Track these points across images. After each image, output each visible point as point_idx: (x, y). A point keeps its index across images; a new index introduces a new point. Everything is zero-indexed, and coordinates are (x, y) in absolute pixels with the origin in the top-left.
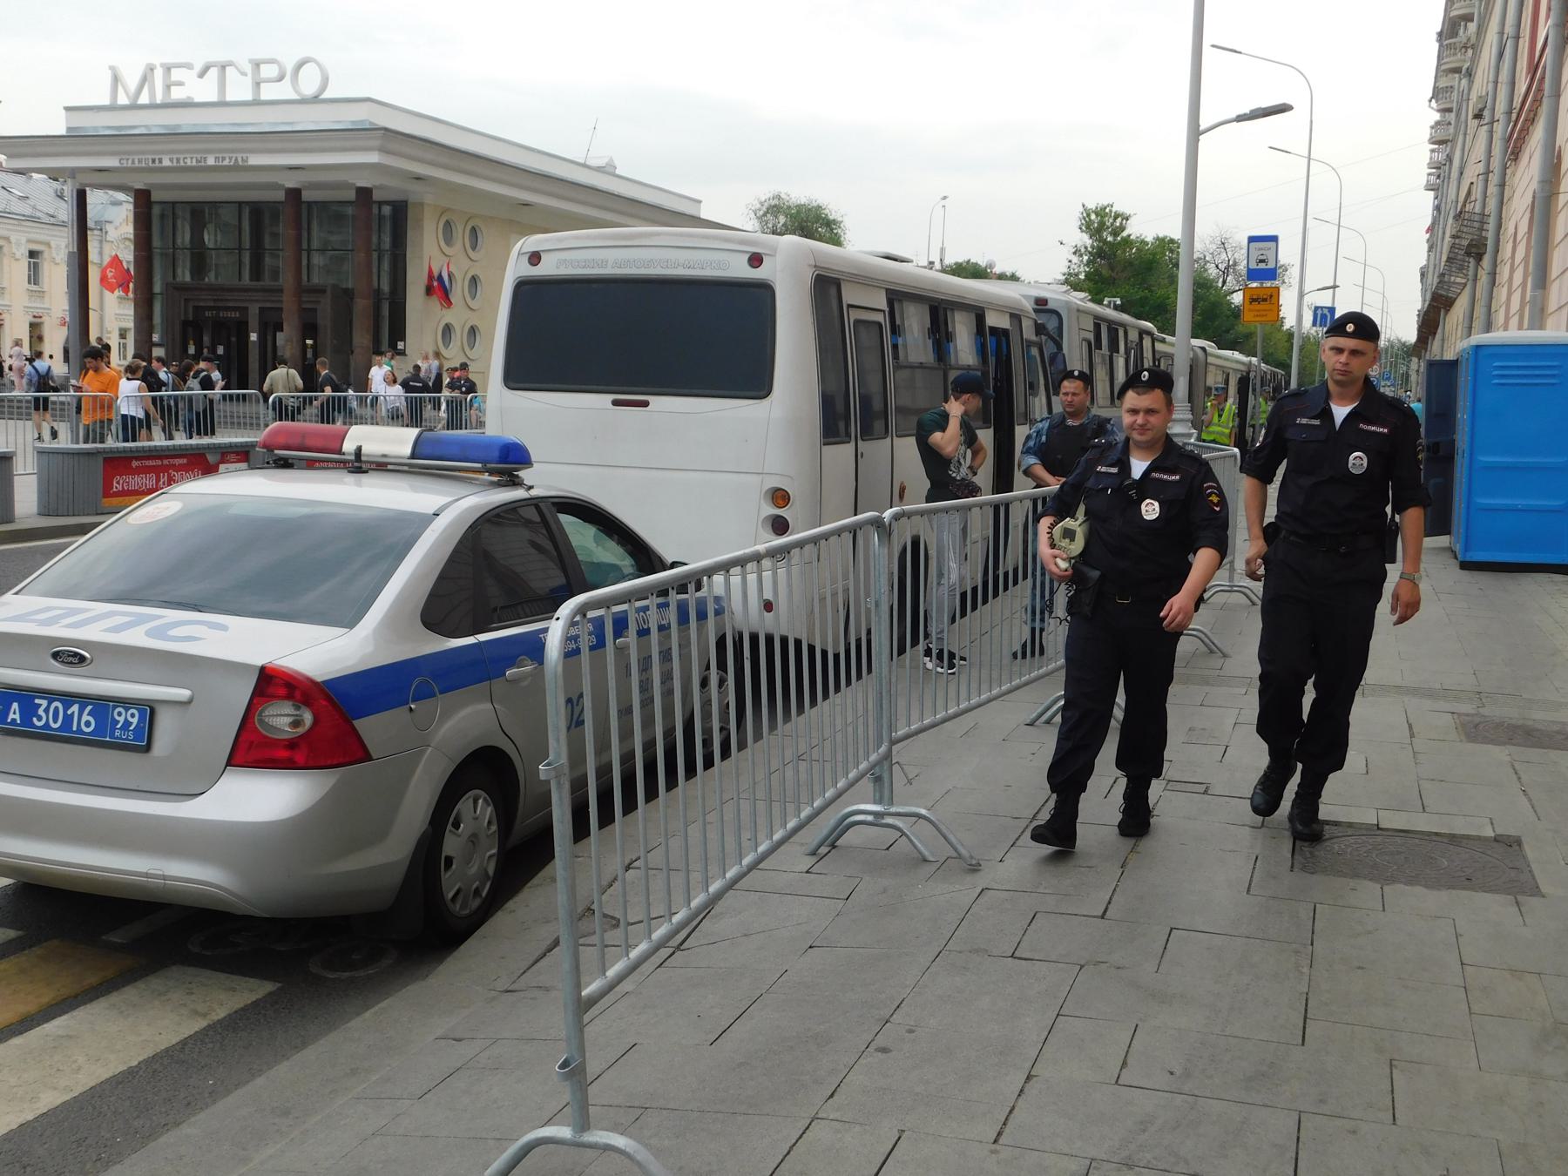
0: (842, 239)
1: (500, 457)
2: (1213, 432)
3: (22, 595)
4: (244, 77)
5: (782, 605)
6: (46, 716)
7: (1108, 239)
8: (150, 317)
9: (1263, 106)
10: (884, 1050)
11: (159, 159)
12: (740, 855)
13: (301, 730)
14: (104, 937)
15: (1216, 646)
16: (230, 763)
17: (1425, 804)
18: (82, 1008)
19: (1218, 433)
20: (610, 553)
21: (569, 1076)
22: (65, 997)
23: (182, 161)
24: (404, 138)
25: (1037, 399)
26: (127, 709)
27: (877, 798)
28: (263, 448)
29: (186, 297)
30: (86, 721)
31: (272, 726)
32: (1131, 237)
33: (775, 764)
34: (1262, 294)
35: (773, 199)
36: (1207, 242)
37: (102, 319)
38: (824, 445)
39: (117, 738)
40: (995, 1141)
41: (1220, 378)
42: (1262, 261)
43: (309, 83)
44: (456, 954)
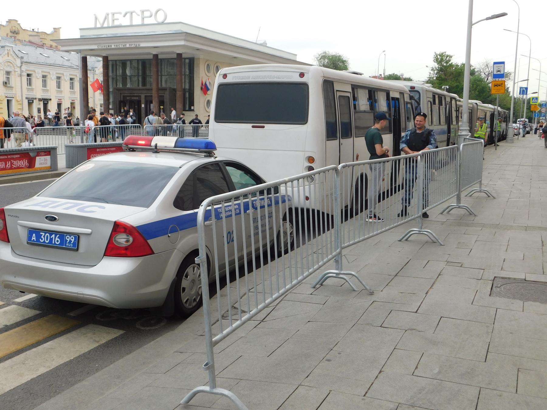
0: (348, 67)
1: (205, 147)
2: (478, 134)
3: (42, 196)
4: (139, 16)
5: (312, 198)
7: (444, 65)
8: (108, 100)
9: (496, 14)
10: (329, 360)
12: (279, 289)
13: (129, 244)
14: (68, 314)
15: (472, 212)
16: (104, 255)
17: (544, 271)
18: (57, 338)
19: (481, 134)
20: (247, 179)
21: (208, 369)
22: (52, 334)
23: (118, 46)
24: (192, 36)
25: (410, 123)
26: (70, 236)
27: (337, 267)
28: (125, 145)
31: (119, 242)
32: (453, 64)
33: (304, 255)
34: (498, 83)
36: (481, 65)
37: (94, 101)
38: (327, 140)
39: (67, 246)
40: (364, 396)
41: (483, 114)
42: (499, 71)
43: (160, 18)
44: (186, 322)
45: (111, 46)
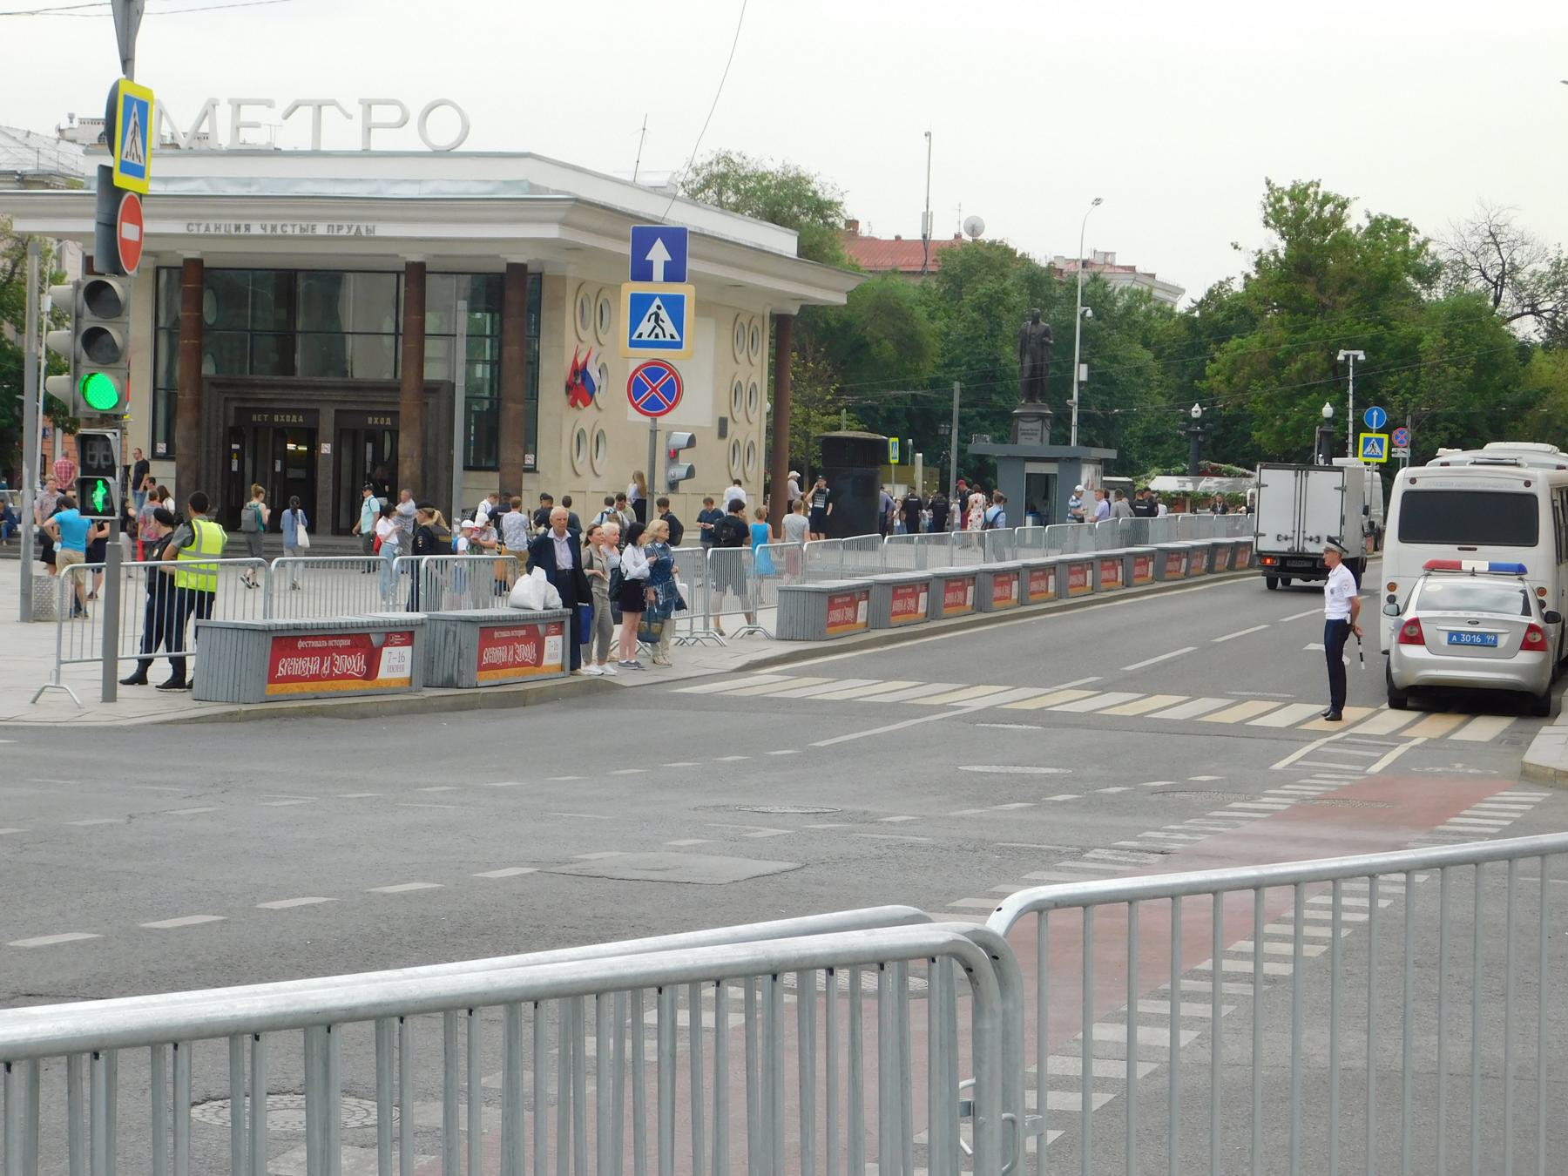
6: (1464, 639)
11: (246, 225)
24: (586, 206)
29: (226, 395)
30: (1478, 640)
35: (718, 163)
36: (1466, 233)
43: (443, 132)
45: (248, 228)
